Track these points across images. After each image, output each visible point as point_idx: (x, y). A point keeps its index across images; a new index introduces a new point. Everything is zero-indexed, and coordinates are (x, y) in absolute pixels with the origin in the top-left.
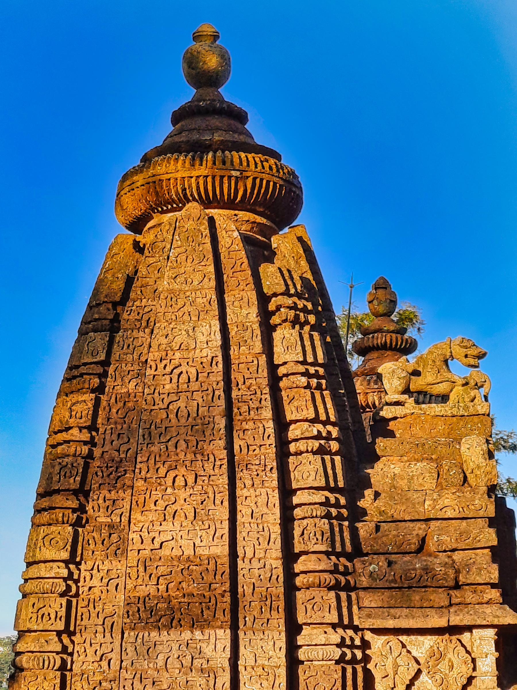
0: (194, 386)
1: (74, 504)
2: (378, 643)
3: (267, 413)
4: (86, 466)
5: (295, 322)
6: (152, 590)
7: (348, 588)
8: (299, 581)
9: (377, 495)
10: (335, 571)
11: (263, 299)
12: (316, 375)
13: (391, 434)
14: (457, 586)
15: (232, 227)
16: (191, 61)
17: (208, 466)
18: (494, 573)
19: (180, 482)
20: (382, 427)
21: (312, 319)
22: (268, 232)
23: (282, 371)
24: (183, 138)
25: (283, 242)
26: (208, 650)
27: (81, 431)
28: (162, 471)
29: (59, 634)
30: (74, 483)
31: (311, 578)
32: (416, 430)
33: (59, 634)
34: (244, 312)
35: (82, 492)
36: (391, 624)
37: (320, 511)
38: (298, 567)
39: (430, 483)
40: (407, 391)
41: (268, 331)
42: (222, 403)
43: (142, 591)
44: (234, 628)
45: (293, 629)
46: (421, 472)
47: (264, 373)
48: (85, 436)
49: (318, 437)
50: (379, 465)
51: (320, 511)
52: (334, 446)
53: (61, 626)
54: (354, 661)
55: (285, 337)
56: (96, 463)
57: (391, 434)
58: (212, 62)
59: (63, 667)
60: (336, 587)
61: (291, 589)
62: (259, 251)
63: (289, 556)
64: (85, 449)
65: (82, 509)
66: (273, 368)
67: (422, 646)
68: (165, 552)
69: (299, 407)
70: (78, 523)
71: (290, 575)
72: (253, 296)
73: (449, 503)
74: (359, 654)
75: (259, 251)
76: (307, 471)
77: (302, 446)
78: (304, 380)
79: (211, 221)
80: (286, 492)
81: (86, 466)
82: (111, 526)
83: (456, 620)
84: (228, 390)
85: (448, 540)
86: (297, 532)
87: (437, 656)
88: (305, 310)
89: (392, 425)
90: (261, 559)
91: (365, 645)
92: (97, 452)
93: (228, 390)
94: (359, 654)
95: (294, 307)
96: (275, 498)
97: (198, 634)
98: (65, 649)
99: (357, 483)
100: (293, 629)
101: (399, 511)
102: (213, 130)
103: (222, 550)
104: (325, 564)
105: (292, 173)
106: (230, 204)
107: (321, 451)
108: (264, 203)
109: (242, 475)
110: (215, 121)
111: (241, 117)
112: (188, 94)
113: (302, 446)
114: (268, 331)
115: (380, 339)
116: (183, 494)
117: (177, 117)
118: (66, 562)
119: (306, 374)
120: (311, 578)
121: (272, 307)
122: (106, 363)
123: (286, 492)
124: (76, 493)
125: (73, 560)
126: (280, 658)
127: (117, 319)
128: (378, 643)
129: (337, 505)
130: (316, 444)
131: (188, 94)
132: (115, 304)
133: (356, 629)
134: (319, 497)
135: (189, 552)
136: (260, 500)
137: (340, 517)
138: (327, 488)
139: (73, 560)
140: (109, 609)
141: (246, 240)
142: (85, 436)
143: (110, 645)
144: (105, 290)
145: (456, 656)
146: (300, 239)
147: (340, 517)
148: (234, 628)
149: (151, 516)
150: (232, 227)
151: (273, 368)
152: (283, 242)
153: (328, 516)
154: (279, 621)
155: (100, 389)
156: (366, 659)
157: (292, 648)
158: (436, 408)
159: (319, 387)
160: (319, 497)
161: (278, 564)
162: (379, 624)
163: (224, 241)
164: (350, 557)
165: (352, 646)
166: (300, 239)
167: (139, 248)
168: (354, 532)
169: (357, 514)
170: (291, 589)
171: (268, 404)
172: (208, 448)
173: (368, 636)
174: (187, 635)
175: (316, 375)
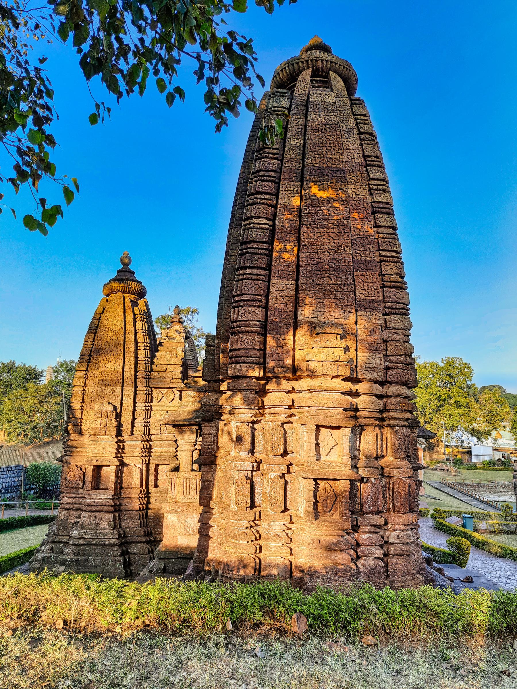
0: (117, 333)
1: (88, 358)
2: (155, 390)
3: (133, 340)
4: (91, 350)
5: (141, 320)
6: (104, 378)
7: (149, 379)
8: (138, 377)
9: (157, 359)
10: (146, 375)
11: (134, 315)
12: (145, 333)
13: (163, 346)
14: (173, 379)
15: (128, 298)
16: (122, 260)
17: (119, 351)
18: (180, 376)
19: (112, 354)
20: (161, 344)
21: (145, 320)
22: (138, 300)
23: (137, 331)
24: (119, 277)
25: (141, 302)
26: (116, 391)
27: (293, 388)
28: (108, 352)
29: (83, 386)
30: (88, 353)
31: (141, 376)
32: (168, 345)
33: (83, 386)
34: (130, 318)
35: (90, 355)
36: (157, 386)
37: (144, 362)
38: (138, 374)
39: (169, 357)
40: (167, 337)
41: (135, 322)
42: (123, 338)
43: (102, 378)
44: (123, 386)
45: (136, 387)
46: (168, 354)
47: (133, 331)
48: (92, 343)
49: (145, 346)
50: (159, 352)
51: (144, 362)
52: (148, 348)
53: (83, 385)
54: (149, 394)
55: (139, 324)
56: (93, 349)
57: (163, 346)
58: (126, 261)
59: (83, 394)
60: (146, 378)
61: (136, 378)
62: (135, 304)
63: (136, 371)
64: (91, 346)
65: (90, 359)
66: (135, 330)
67: (164, 391)
68: (108, 369)
69: (140, 339)
70: (89, 362)
71: (136, 376)
72: (132, 314)
73: (173, 361)
74: (150, 393)
75: (135, 304)
76: (141, 353)
77: (141, 348)
78: (142, 333)
79: (124, 297)
80: (136, 357)
81: (91, 350)
82: (96, 363)
83: (171, 386)
84: (125, 335)
85: (172, 369)
86: (138, 366)
87: (167, 393)
88: (144, 318)
89: (163, 344)
90: (129, 372)
91: (152, 391)
92: (94, 347)
93: (125, 335)
94: (150, 393)
95: (141, 317)
96: (134, 359)
97: (114, 388)
98: (84, 390)
99: (153, 356)
100: (136, 387)
101: (162, 363)
102: (126, 276)
103: (121, 369)
104: (144, 373)
105: (144, 287)
106: (129, 293)
107: (145, 349)
108: (137, 293)
109: (127, 353)
110: (127, 274)
111: (133, 273)
112: (121, 266)
113: (141, 348)
114: (135, 322)
115: (175, 320)
116: (113, 357)
117: (119, 272)
118: (89, 356)
119: (143, 332)
120: (141, 376)
121: (136, 317)
122: (97, 327)
123: (136, 357)
124: (89, 356)
125: (87, 370)
126: (132, 393)
127: (100, 317)
128: (155, 390)
129: (148, 361)
130: (144, 348)
131: (121, 266)
132: (100, 314)
133: (150, 387)
134: (144, 359)
135: (113, 370)
136: (130, 360)
137: (148, 363)
138: (146, 357)
139: (87, 370)
140: (94, 381)
141: (132, 301)
142: (92, 343)
143: (95, 389)
144: (98, 311)
145: (171, 393)
146: (145, 302)
147: (148, 363)
148: (123, 386)
149: (105, 362)
150: (128, 298)
151: (135, 330)
152: (141, 302)
153: (145, 363)
154: (133, 385)
155: (96, 333)
156: (152, 393)
157: (135, 391)
158: (173, 341)
159: (146, 335)
160: (144, 359)
161: (133, 373)
162: (155, 386)
163: (126, 301)
164: (150, 372)
165: (149, 391)
166: (145, 302)
167: (107, 301)
168: (151, 367)
169: (152, 363)
170: (136, 378)
171: (133, 338)
172: (119, 347)
173: (153, 389)
174: (112, 388)
175: (145, 333)
